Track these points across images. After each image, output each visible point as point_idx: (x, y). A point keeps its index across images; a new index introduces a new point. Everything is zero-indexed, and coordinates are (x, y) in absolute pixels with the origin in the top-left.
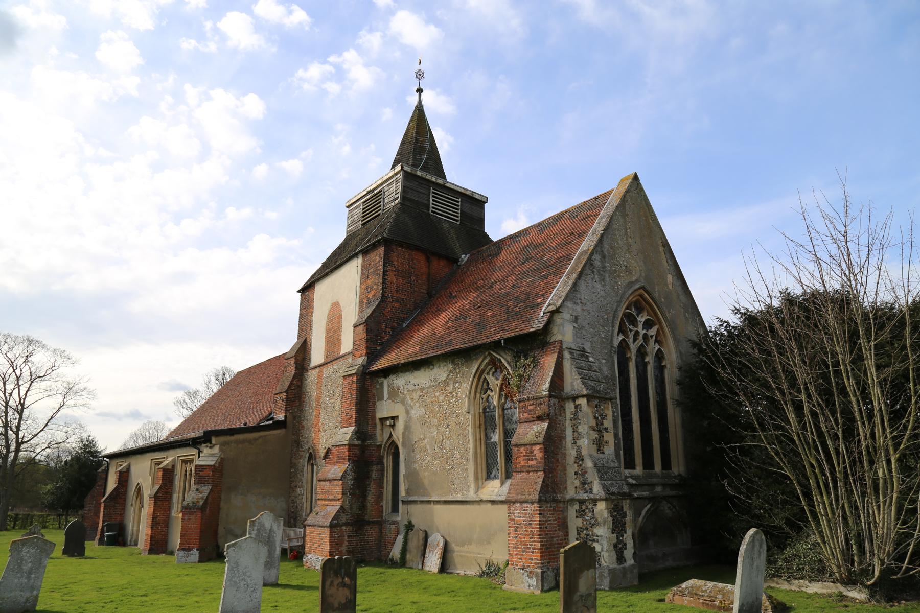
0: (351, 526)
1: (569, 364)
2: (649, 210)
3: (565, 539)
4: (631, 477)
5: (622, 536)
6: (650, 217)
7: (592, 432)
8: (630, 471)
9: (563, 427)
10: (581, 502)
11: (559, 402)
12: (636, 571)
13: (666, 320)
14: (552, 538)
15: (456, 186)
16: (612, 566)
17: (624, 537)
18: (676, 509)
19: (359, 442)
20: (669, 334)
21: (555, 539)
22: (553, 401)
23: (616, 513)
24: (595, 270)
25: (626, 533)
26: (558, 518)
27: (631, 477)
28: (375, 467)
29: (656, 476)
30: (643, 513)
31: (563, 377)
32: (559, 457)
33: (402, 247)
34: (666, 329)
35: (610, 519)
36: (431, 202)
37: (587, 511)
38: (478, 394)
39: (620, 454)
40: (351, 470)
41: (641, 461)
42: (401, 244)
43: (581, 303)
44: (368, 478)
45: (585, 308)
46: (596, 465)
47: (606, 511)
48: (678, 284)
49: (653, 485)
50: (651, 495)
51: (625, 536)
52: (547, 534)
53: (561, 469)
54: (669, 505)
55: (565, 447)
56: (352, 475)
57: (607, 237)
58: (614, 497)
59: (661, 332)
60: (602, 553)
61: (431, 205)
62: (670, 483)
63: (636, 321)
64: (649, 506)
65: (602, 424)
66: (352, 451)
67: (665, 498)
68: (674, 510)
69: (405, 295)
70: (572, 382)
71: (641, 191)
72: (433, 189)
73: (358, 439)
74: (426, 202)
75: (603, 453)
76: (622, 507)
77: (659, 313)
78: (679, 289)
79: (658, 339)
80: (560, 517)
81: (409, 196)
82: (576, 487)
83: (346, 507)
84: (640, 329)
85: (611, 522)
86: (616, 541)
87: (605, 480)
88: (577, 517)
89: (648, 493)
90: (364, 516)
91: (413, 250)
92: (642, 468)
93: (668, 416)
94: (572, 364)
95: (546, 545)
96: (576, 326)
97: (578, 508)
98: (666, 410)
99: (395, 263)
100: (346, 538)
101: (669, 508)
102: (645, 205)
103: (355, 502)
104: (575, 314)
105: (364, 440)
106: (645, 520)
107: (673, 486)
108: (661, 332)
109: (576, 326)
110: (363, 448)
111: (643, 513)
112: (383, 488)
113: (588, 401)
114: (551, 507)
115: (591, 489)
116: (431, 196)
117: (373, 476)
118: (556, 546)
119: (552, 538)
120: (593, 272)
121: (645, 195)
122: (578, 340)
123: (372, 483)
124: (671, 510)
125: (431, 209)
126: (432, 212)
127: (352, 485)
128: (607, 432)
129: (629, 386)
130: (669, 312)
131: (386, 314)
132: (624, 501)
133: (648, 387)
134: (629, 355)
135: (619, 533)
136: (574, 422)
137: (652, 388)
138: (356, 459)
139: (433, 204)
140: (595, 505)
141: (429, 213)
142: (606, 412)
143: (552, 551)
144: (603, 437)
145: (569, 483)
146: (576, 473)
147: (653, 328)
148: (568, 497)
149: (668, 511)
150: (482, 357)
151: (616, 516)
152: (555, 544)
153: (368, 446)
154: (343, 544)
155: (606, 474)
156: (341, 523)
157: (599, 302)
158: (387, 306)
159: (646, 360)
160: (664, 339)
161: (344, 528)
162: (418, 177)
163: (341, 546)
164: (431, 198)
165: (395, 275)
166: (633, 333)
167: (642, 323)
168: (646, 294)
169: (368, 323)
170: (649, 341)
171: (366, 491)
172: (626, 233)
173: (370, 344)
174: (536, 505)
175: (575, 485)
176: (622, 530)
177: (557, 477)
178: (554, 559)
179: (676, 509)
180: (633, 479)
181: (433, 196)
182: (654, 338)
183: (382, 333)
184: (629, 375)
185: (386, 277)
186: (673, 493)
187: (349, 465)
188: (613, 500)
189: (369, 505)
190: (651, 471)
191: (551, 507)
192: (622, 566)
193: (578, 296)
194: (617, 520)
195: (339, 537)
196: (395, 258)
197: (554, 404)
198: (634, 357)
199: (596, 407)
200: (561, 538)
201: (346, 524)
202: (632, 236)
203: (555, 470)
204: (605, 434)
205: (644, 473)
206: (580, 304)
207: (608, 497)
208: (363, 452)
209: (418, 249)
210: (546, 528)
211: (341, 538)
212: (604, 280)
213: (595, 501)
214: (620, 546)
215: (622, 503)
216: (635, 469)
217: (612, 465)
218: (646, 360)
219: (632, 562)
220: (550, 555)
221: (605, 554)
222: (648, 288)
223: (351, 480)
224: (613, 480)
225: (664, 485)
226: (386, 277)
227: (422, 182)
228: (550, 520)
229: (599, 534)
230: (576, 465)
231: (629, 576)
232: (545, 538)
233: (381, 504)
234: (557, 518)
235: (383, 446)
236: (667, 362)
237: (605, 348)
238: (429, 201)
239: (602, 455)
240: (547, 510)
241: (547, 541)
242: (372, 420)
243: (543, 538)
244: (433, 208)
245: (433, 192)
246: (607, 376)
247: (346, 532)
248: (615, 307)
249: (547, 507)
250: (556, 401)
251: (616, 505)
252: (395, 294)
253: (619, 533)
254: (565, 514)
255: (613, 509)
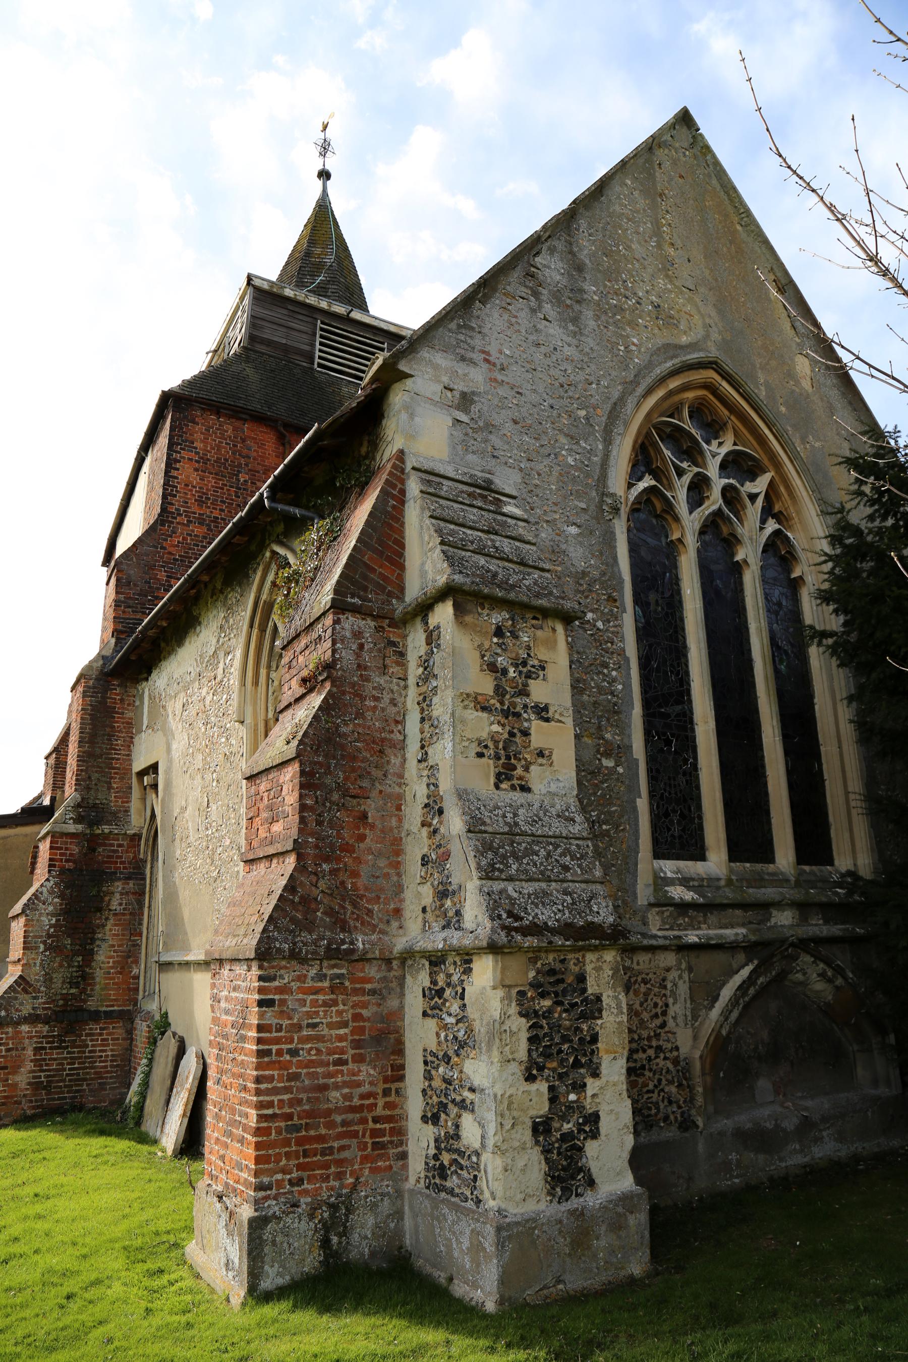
0: (46, 1022)
1: (418, 510)
2: (731, 200)
3: (386, 1092)
4: (685, 882)
5: (580, 1087)
6: (736, 219)
7: (472, 715)
8: (682, 864)
9: (393, 710)
10: (436, 960)
11: (378, 629)
12: (639, 1220)
13: (794, 457)
14: (324, 1088)
15: (376, 318)
16: (517, 1211)
17: (590, 1091)
18: (845, 978)
19: (80, 827)
20: (804, 494)
21: (335, 1095)
22: (350, 622)
23: (547, 1003)
24: (545, 292)
25: (596, 1075)
26: (357, 1017)
27: (685, 882)
28: (119, 886)
29: (780, 880)
30: (727, 993)
31: (401, 555)
32: (371, 807)
33: (218, 414)
34: (797, 482)
35: (520, 1025)
36: (318, 346)
37: (448, 992)
38: (263, 672)
39: (635, 809)
40: (51, 892)
41: (722, 835)
42: (216, 408)
43: (487, 361)
44: (100, 910)
45: (500, 377)
46: (474, 827)
47: (500, 993)
48: (829, 382)
49: (765, 907)
50: (753, 938)
51: (592, 1086)
52: (295, 1077)
53: (376, 846)
54: (822, 965)
55: (401, 776)
56: (54, 905)
57: (590, 226)
58: (531, 941)
59: (782, 489)
60: (484, 1158)
61: (317, 353)
62: (824, 899)
63: (701, 452)
64: (745, 972)
65: (524, 692)
66: (60, 848)
67: (803, 944)
68: (839, 981)
69: (222, 510)
70: (423, 564)
71: (705, 155)
72: (322, 323)
73: (78, 820)
74: (307, 348)
75: (525, 789)
76: (581, 978)
77: (771, 437)
78: (835, 395)
79: (777, 508)
80: (365, 1013)
81: (267, 334)
82: (424, 910)
83: (32, 978)
84: (712, 470)
85: (524, 1036)
86: (545, 1108)
87: (510, 879)
88: (425, 1014)
89: (742, 931)
90: (85, 1001)
91: (245, 420)
92: (724, 855)
93: (817, 715)
94: (422, 509)
95: (289, 1117)
96: (464, 418)
97: (427, 983)
98: (811, 696)
99: (199, 445)
100: (30, 1052)
101: (822, 975)
102: (718, 187)
103: (61, 966)
104: (460, 386)
105: (91, 824)
106: (735, 1015)
107: (831, 911)
108: (782, 489)
109: (464, 418)
110: (92, 843)
111: (727, 993)
112: (141, 935)
113: (459, 610)
114: (321, 977)
115: (458, 913)
116: (318, 336)
117: (114, 905)
118: (338, 1119)
119: (324, 1088)
120: (536, 294)
121: (717, 163)
122: (470, 457)
123: (112, 921)
124: (830, 981)
125: (317, 360)
126: (320, 365)
127: (51, 926)
128: (547, 720)
129: (682, 620)
130: (804, 440)
131: (171, 549)
132: (590, 957)
133: (747, 629)
134: (675, 536)
135: (561, 1077)
136: (424, 689)
137: (760, 630)
138: (70, 865)
139: (320, 351)
140: (468, 971)
141: (312, 369)
142: (542, 653)
143: (321, 1139)
144: (526, 733)
145: (408, 894)
146: (425, 861)
147: (759, 479)
148: (400, 944)
149: (819, 986)
150: (261, 568)
151: (550, 1011)
152: (338, 1110)
153: (106, 837)
154: (19, 1067)
155: (517, 858)
156: (15, 1016)
157: (556, 373)
158: (174, 532)
159: (739, 557)
160: (792, 509)
161: (25, 1028)
162: (288, 299)
163: (15, 1073)
164: (318, 340)
165: (196, 470)
166: (687, 479)
167: (719, 459)
168: (724, 384)
169: (124, 567)
170: (744, 507)
171: (93, 940)
172: (657, 232)
173: (124, 612)
174: (255, 966)
175: (423, 903)
176: (577, 1064)
177: (355, 874)
178: (326, 1166)
179: (845, 978)
180: (689, 888)
181: (321, 336)
182: (760, 501)
183: (159, 589)
184: (679, 592)
185: (174, 473)
186: (836, 930)
187: (47, 880)
188: (534, 955)
189: (99, 974)
190: (759, 866)
191: (321, 977)
192: (574, 1203)
193: (477, 342)
194: (555, 1027)
195: (8, 1050)
196: (198, 436)
197: (357, 634)
198: (691, 542)
199: (499, 632)
200: (366, 1088)
201: (32, 1019)
202: (679, 244)
203: (348, 849)
204: (536, 726)
205: (731, 871)
206: (485, 366)
207: (502, 938)
208: (93, 850)
209: (259, 419)
210: (294, 1053)
211: (14, 1053)
212: (575, 320)
213: (466, 957)
214: (567, 1127)
215: (580, 962)
216: (702, 858)
217: (558, 827)
218: (739, 557)
219: (627, 1182)
220: (306, 1154)
221: (491, 1163)
222: (729, 365)
223: (53, 915)
224: (549, 880)
225: (803, 908)
226: (174, 473)
227: (297, 310)
228: (314, 1026)
229: (476, 1083)
230: (425, 832)
231: (603, 1242)
232: (287, 1090)
233: (135, 971)
234: (348, 1016)
235: (144, 836)
236: (806, 569)
237: (579, 495)
238: (313, 346)
239: (518, 797)
240: (301, 990)
241: (292, 1103)
242: (122, 779)
243: (275, 1091)
244: (320, 357)
245: (322, 329)
246: (584, 574)
247: (31, 1038)
248: (616, 395)
249: (302, 978)
250: (367, 625)
251: (552, 972)
252: (195, 508)
253: (561, 1077)
254: (393, 1003)
255: (535, 985)
